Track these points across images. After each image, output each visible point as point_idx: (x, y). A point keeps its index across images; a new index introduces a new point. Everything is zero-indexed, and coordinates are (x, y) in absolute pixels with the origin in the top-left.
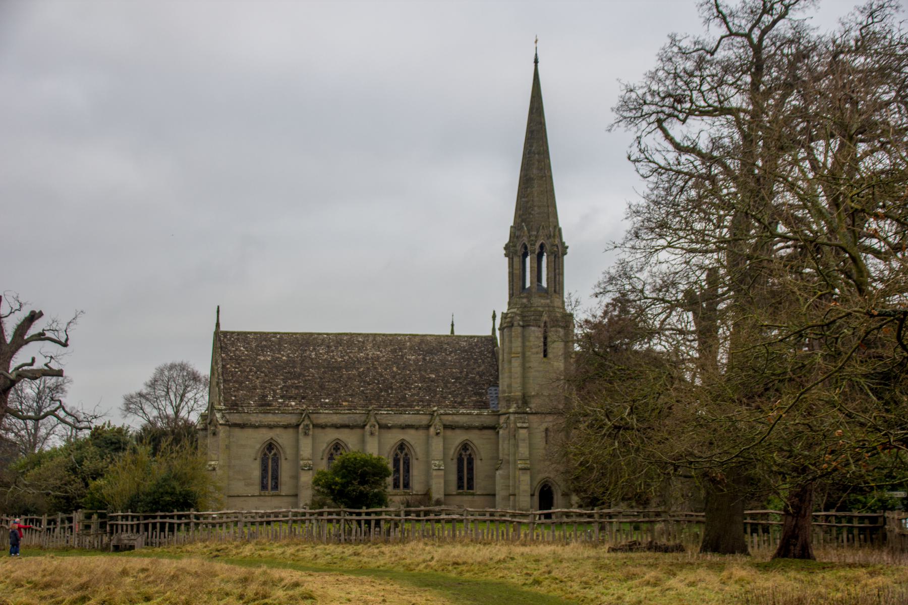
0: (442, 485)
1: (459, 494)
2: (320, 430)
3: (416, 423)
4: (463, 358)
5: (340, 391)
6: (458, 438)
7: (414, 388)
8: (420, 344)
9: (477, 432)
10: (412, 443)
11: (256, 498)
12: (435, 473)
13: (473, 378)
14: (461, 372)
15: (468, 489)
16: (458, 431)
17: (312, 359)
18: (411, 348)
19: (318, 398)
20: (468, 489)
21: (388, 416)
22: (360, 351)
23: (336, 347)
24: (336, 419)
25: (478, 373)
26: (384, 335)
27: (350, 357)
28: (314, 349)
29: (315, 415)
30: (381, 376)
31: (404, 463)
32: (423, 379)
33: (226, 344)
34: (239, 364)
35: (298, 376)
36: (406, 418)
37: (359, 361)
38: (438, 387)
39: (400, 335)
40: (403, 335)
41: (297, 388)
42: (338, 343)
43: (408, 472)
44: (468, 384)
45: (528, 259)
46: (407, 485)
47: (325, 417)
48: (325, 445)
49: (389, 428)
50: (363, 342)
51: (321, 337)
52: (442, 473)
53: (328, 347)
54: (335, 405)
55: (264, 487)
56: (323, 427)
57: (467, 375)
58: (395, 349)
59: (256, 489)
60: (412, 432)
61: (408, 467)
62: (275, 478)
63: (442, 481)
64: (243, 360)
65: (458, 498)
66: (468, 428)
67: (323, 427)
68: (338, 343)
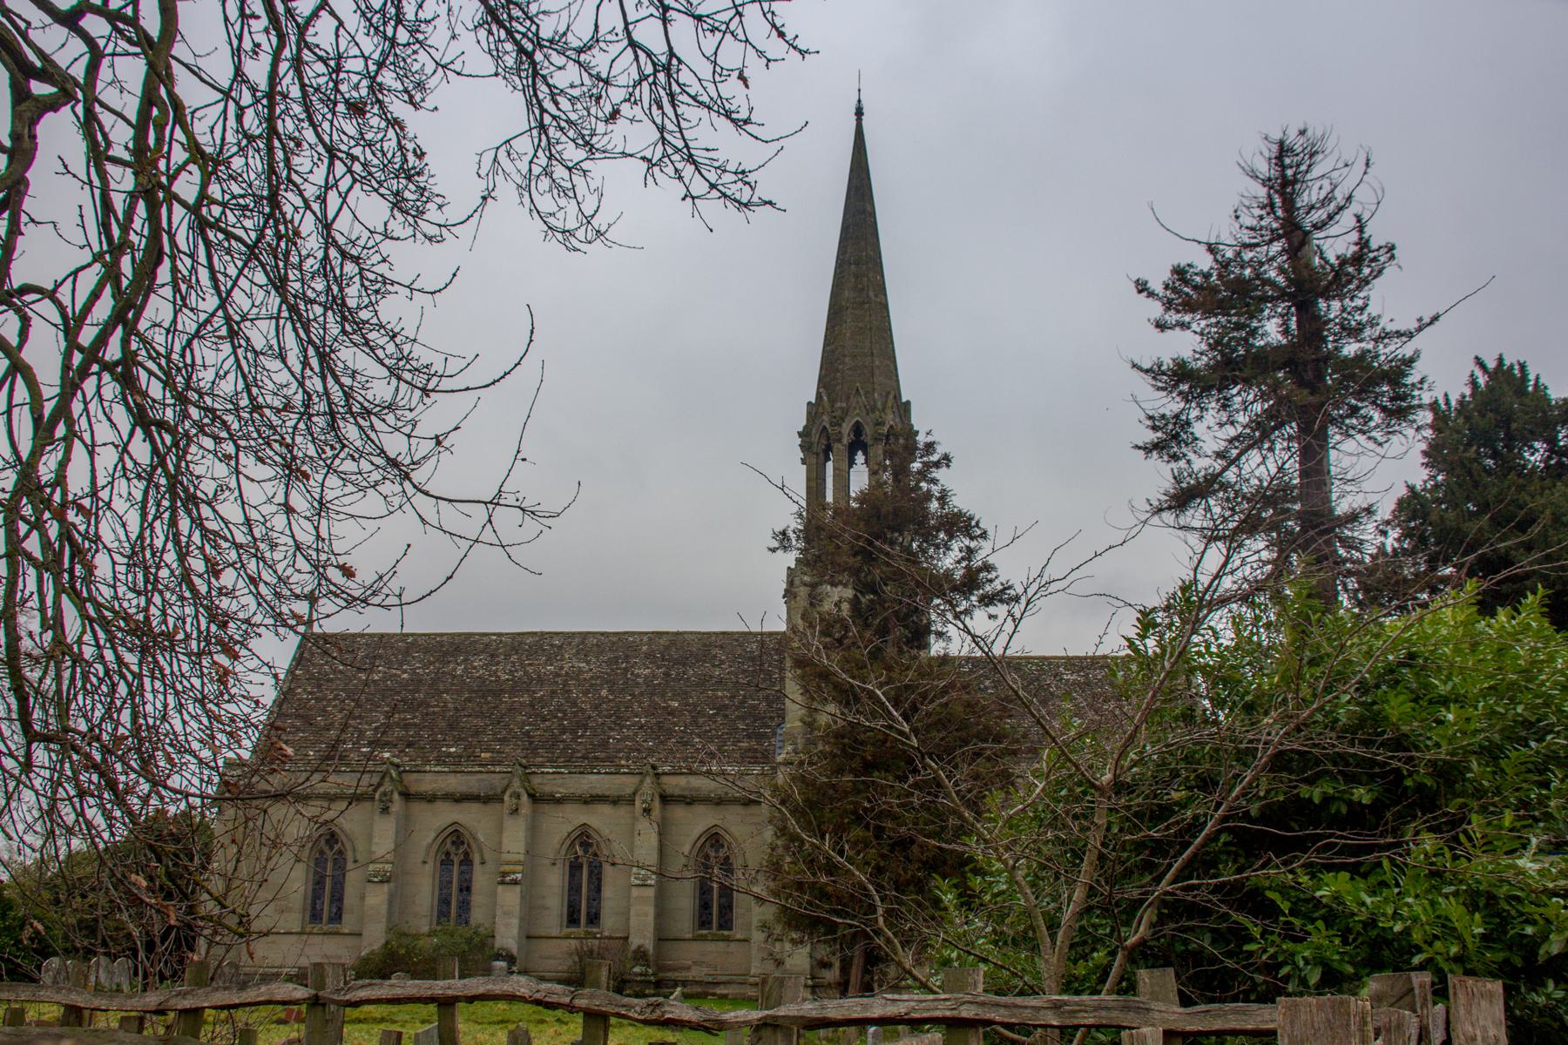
0: (651, 919)
1: (703, 938)
2: (424, 806)
3: (613, 793)
4: (745, 671)
5: (484, 732)
6: (693, 824)
7: (629, 728)
8: (667, 648)
9: (739, 809)
10: (605, 832)
11: (293, 938)
12: (635, 892)
13: (754, 707)
14: (732, 697)
15: (721, 927)
16: (699, 809)
17: (454, 677)
18: (648, 656)
19: (436, 745)
20: (721, 927)
21: (552, 781)
22: (549, 661)
23: (507, 656)
24: (454, 783)
25: (766, 698)
26: (602, 634)
27: (526, 673)
28: (465, 660)
29: (415, 776)
30: (574, 704)
31: (591, 873)
32: (651, 711)
33: (312, 654)
34: (319, 686)
35: (412, 707)
36: (595, 782)
37: (541, 680)
38: (675, 724)
39: (633, 633)
40: (640, 633)
41: (407, 726)
42: (513, 648)
43: (599, 890)
44: (742, 718)
45: (830, 466)
46: (594, 919)
47: (432, 780)
48: (433, 835)
49: (559, 801)
50: (560, 647)
51: (486, 640)
52: (651, 892)
53: (492, 656)
54: (454, 764)
55: (315, 916)
56: (431, 798)
57: (743, 702)
58: (617, 658)
59: (293, 921)
60: (606, 809)
61: (600, 880)
62: (338, 898)
63: (651, 910)
64: (329, 680)
65: (696, 947)
66: (720, 802)
67: (431, 798)
68: (513, 648)
